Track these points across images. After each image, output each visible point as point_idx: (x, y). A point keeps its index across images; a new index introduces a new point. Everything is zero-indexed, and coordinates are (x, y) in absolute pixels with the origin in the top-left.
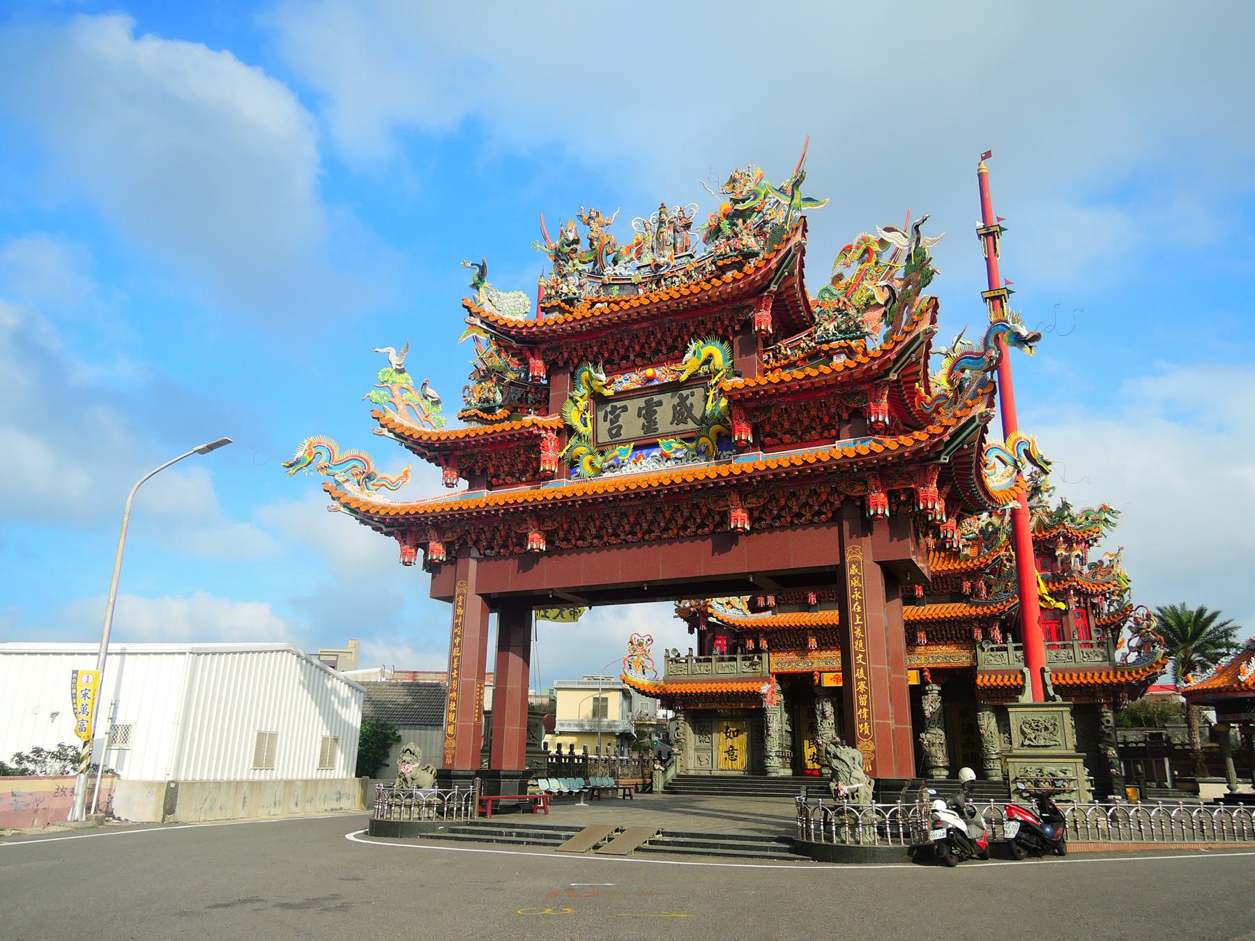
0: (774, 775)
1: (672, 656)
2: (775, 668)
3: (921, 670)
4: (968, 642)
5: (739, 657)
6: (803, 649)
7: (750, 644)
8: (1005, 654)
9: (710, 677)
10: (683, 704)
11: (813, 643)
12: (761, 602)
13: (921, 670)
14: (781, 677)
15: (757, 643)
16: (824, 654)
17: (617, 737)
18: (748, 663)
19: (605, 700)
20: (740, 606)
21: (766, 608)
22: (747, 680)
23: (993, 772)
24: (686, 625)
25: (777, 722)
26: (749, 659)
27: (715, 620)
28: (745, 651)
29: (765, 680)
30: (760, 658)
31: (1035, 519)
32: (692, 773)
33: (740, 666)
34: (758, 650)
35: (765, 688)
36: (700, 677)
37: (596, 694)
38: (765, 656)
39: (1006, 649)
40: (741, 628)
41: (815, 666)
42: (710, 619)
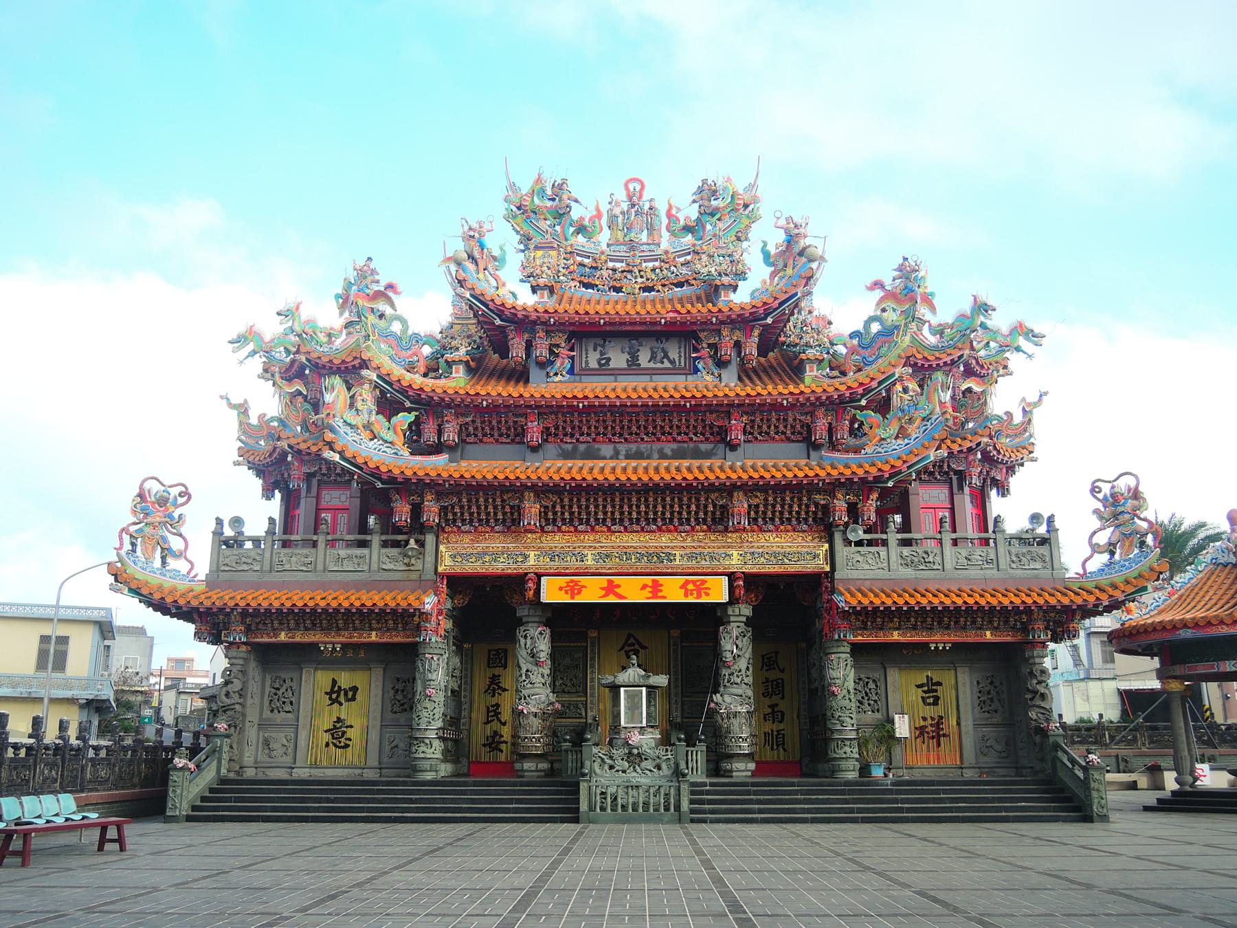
0: (429, 776)
1: (228, 532)
2: (447, 564)
3: (732, 577)
4: (825, 527)
5: (376, 540)
6: (512, 524)
7: (402, 512)
8: (883, 551)
9: (310, 577)
10: (248, 630)
11: (532, 510)
12: (430, 435)
13: (732, 577)
14: (456, 583)
15: (417, 511)
16: (557, 541)
17: (82, 707)
18: (394, 552)
19: (63, 640)
20: (390, 436)
21: (436, 449)
22: (390, 585)
23: (843, 764)
24: (258, 483)
25: (438, 671)
26: (396, 544)
27: (337, 458)
28: (388, 526)
29: (423, 586)
30: (421, 544)
31: (909, 335)
32: (250, 773)
33: (379, 559)
34: (418, 527)
35: (429, 602)
36: (288, 577)
37: (47, 630)
38: (430, 539)
39: (885, 543)
40: (392, 480)
41: (532, 561)
42: (328, 454)
